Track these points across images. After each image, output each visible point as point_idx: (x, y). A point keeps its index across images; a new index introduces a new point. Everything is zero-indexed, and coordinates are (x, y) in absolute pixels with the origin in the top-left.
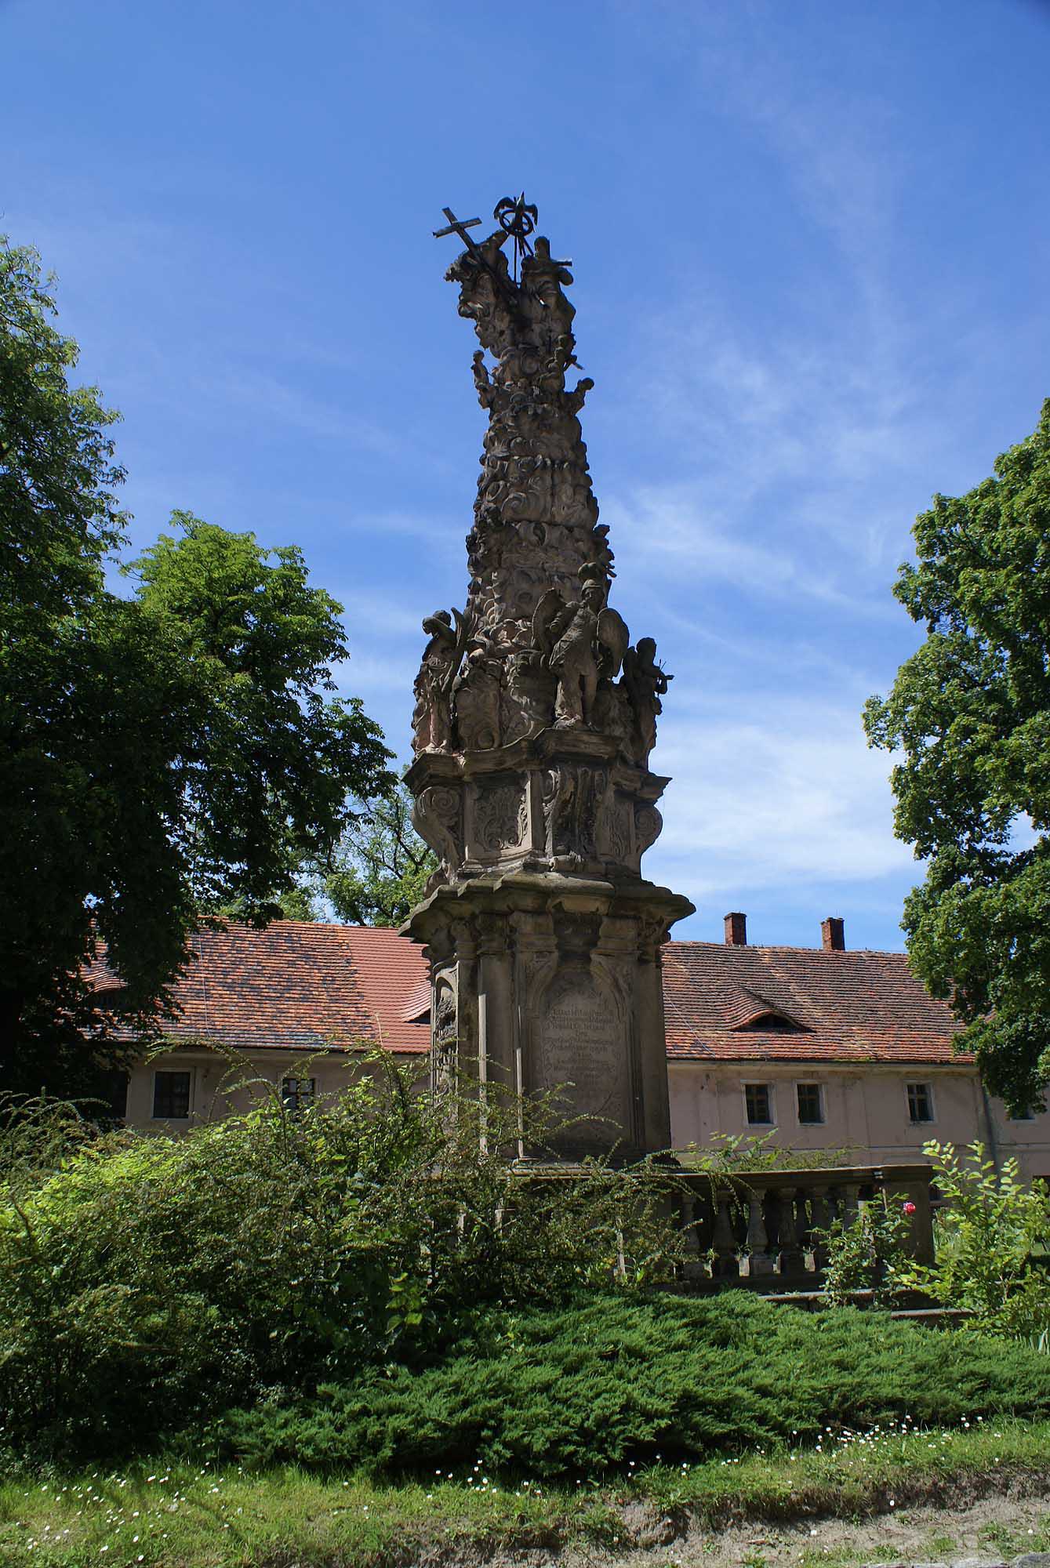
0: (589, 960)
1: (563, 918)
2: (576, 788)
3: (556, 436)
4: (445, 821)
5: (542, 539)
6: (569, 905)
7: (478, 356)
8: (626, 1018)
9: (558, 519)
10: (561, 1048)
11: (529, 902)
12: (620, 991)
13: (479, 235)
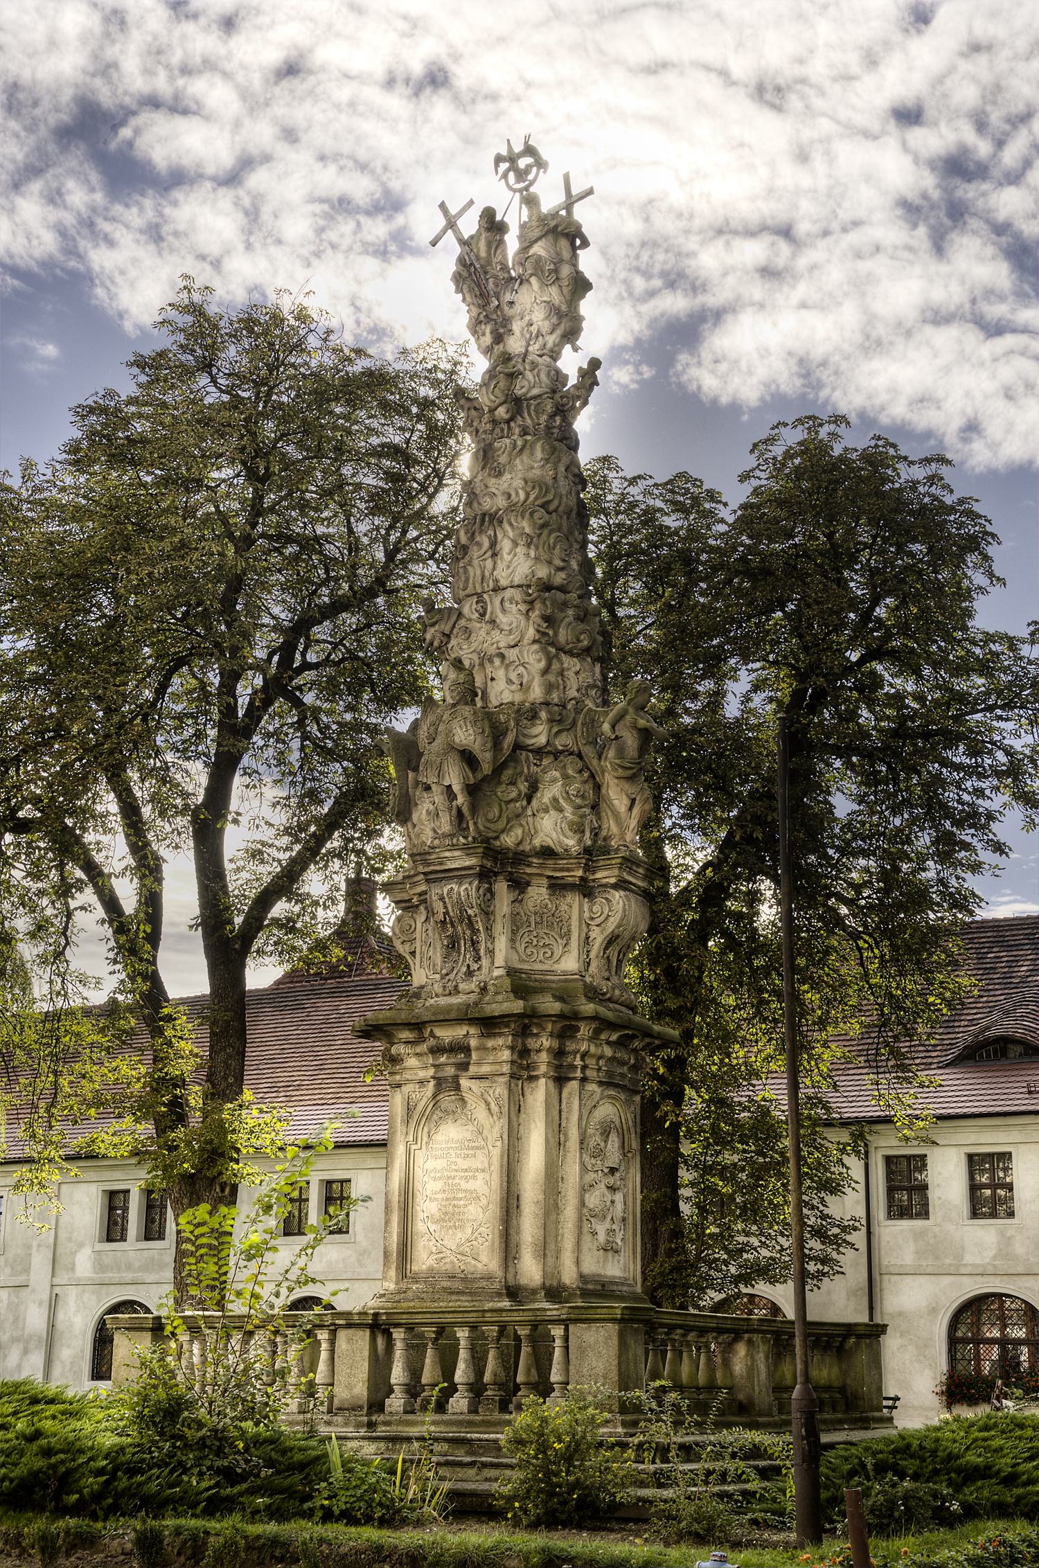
0: (458, 1088)
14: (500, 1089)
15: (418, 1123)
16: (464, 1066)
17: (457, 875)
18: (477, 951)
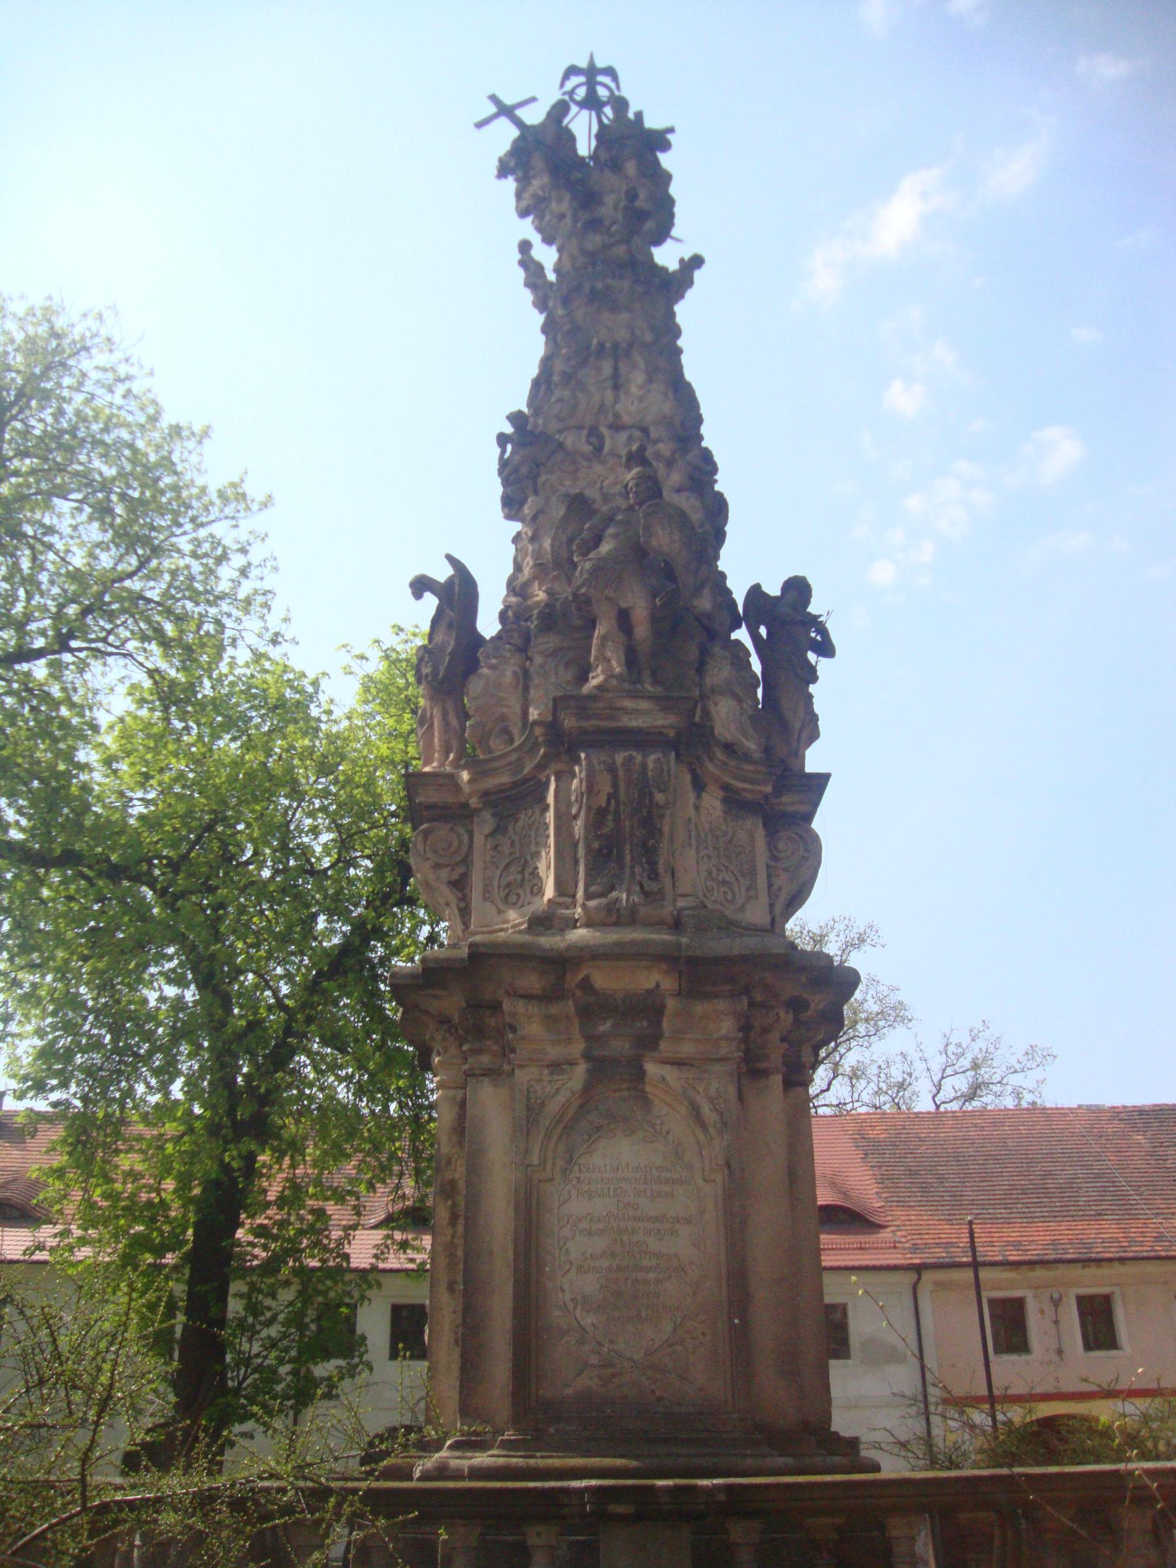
0: (641, 1075)
1: (595, 1005)
2: (615, 785)
3: (624, 316)
4: (444, 874)
5: (599, 449)
6: (602, 980)
7: (525, 246)
8: (719, 1178)
9: (626, 419)
10: (590, 1233)
11: (532, 981)
12: (703, 1125)
13: (534, 116)
14: (718, 1083)
15: (548, 1137)
16: (649, 1042)
17: (118, 984)
18: (653, 864)
